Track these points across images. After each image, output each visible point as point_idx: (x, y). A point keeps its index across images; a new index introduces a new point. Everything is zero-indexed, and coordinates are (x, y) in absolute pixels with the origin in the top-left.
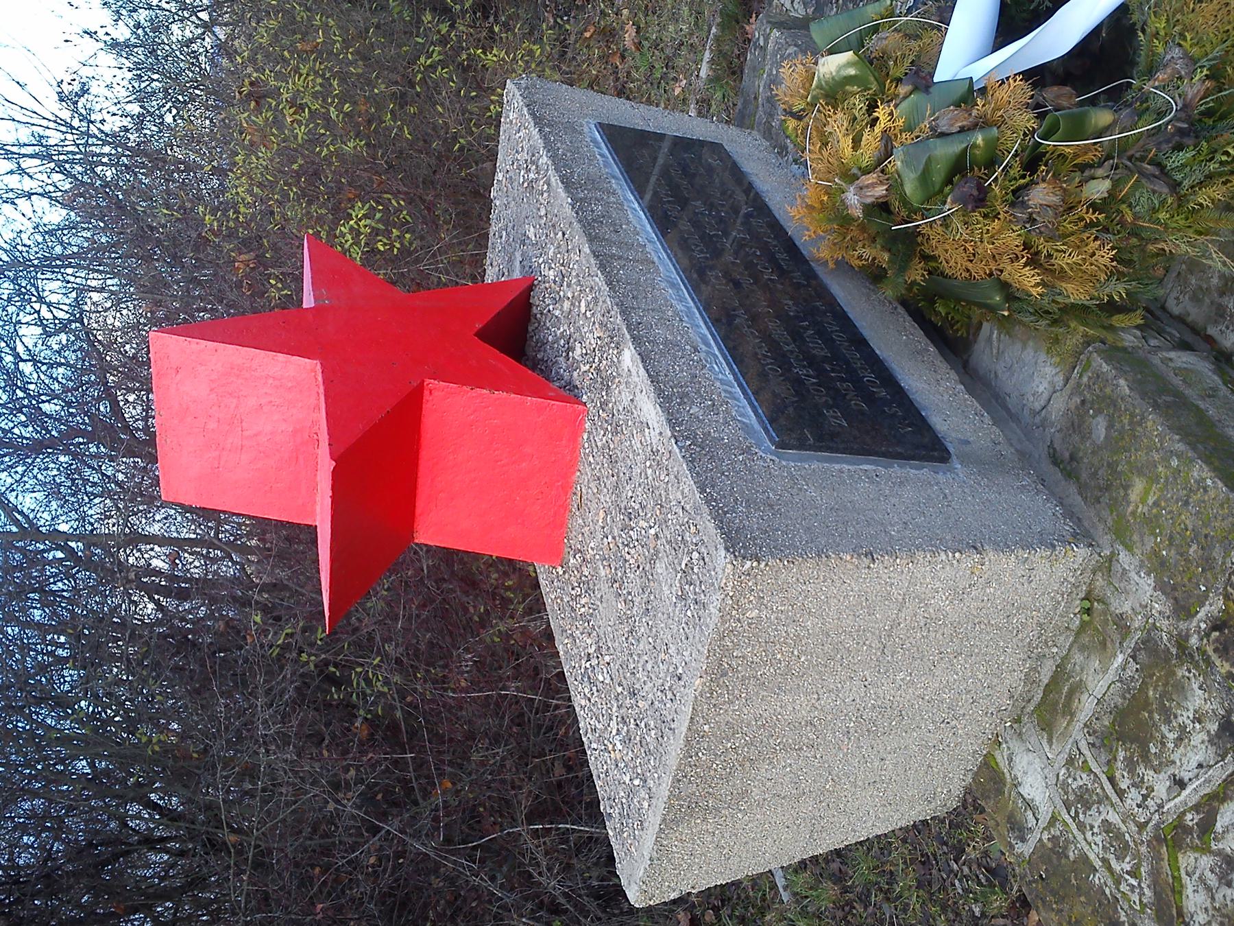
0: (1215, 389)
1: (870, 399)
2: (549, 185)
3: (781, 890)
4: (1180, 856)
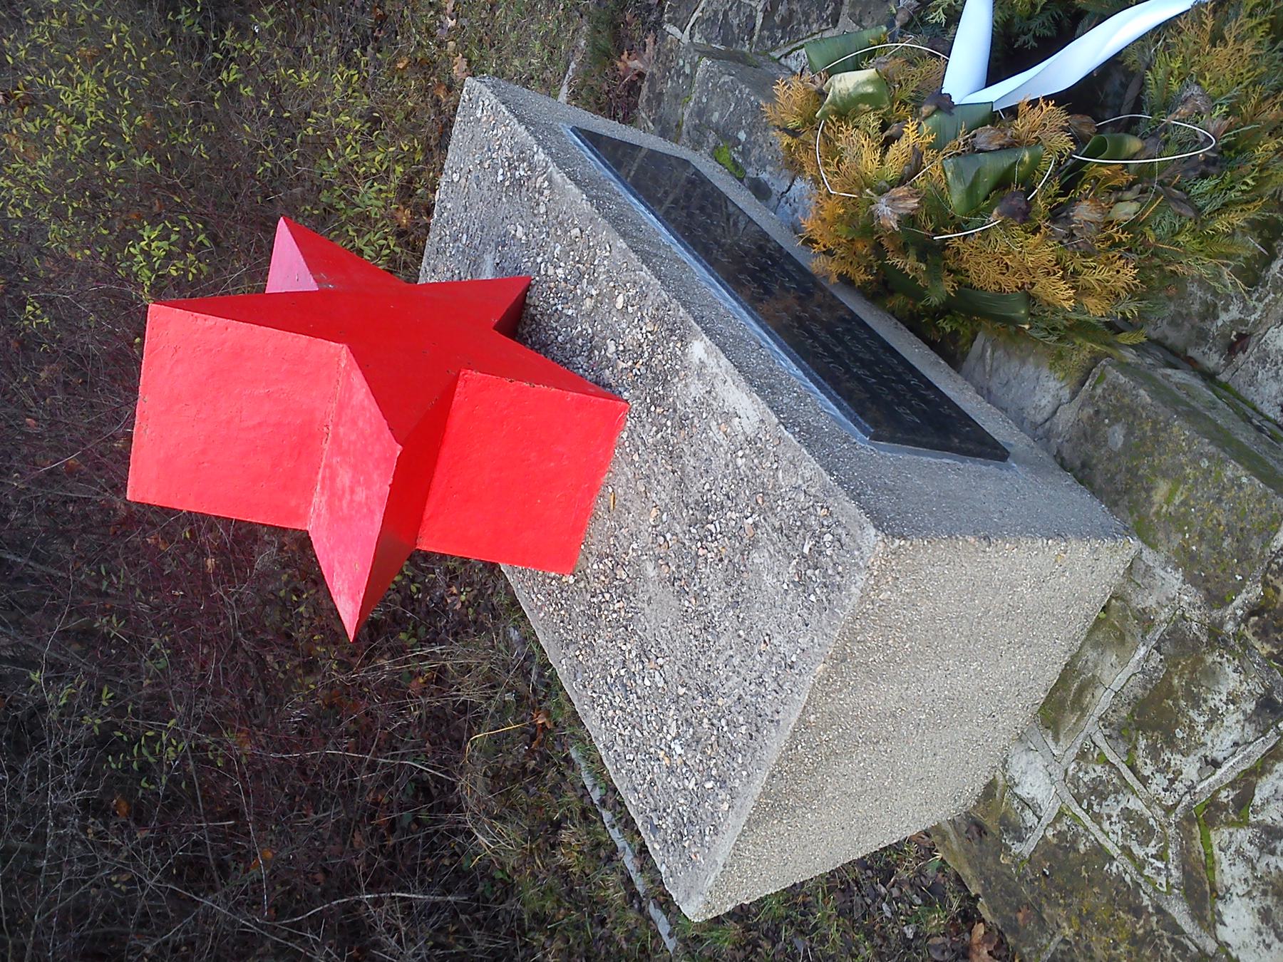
0: (1214, 403)
1: (927, 402)
2: (550, 182)
3: (665, 938)
4: (1212, 833)
